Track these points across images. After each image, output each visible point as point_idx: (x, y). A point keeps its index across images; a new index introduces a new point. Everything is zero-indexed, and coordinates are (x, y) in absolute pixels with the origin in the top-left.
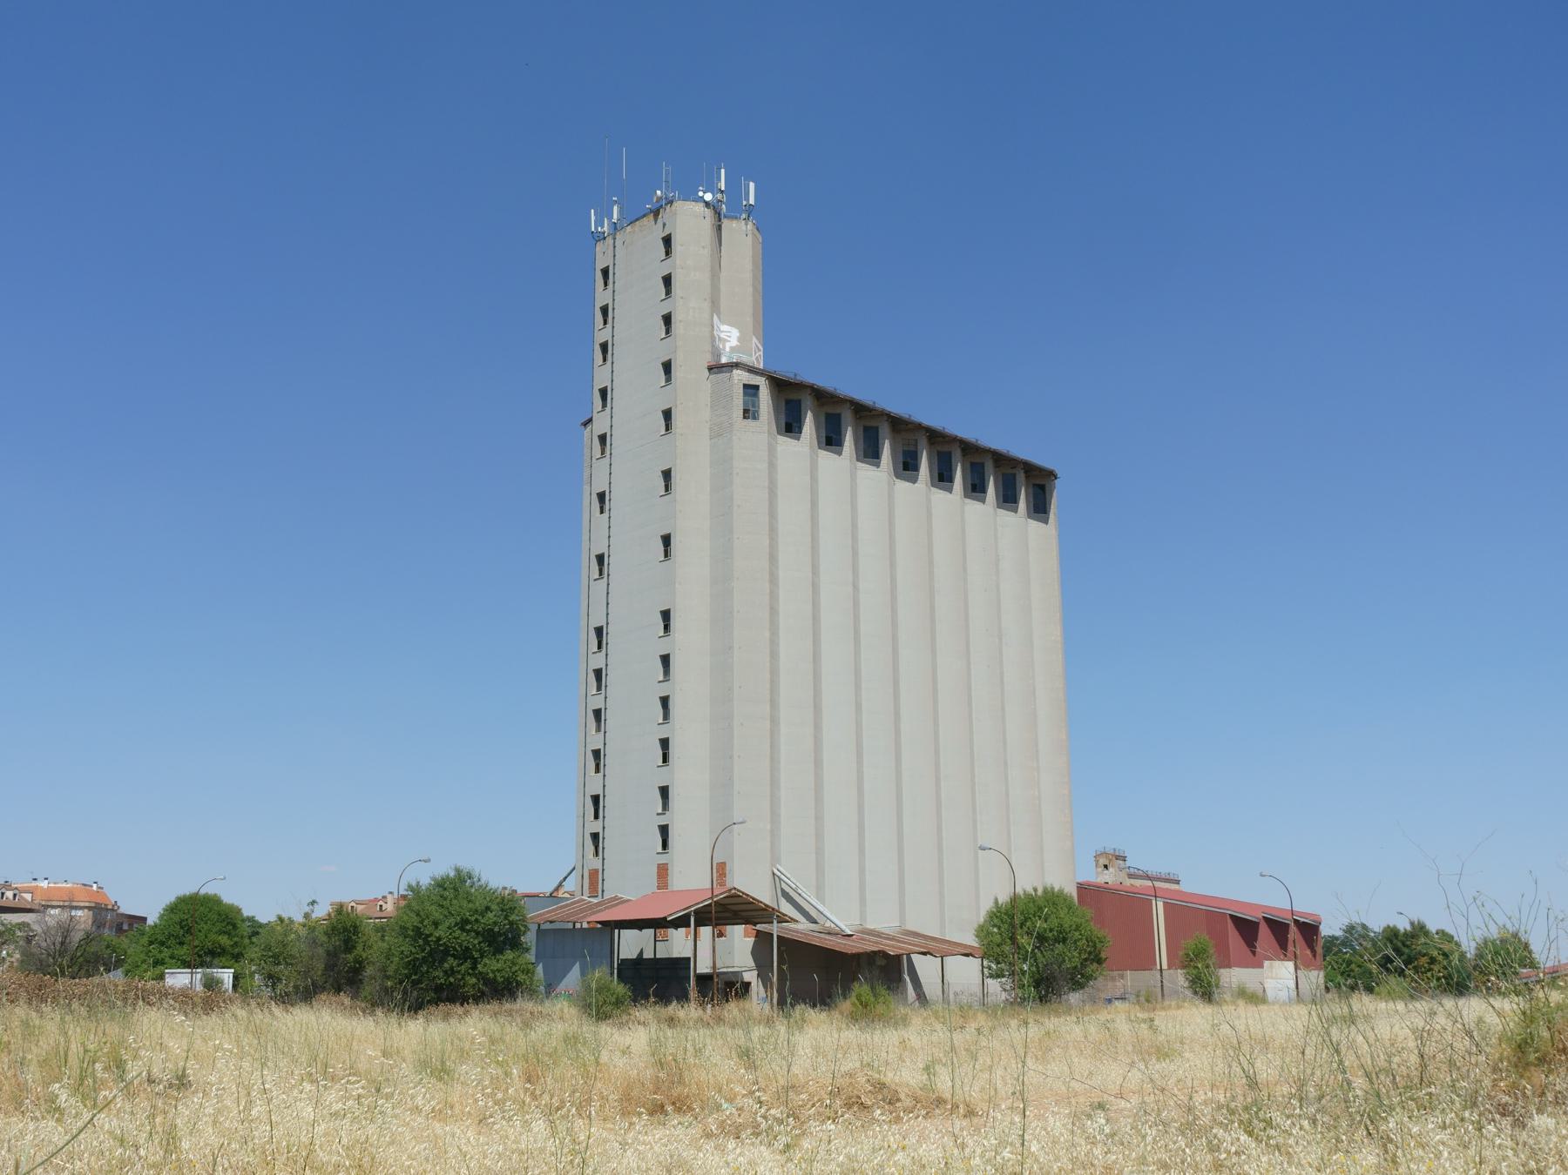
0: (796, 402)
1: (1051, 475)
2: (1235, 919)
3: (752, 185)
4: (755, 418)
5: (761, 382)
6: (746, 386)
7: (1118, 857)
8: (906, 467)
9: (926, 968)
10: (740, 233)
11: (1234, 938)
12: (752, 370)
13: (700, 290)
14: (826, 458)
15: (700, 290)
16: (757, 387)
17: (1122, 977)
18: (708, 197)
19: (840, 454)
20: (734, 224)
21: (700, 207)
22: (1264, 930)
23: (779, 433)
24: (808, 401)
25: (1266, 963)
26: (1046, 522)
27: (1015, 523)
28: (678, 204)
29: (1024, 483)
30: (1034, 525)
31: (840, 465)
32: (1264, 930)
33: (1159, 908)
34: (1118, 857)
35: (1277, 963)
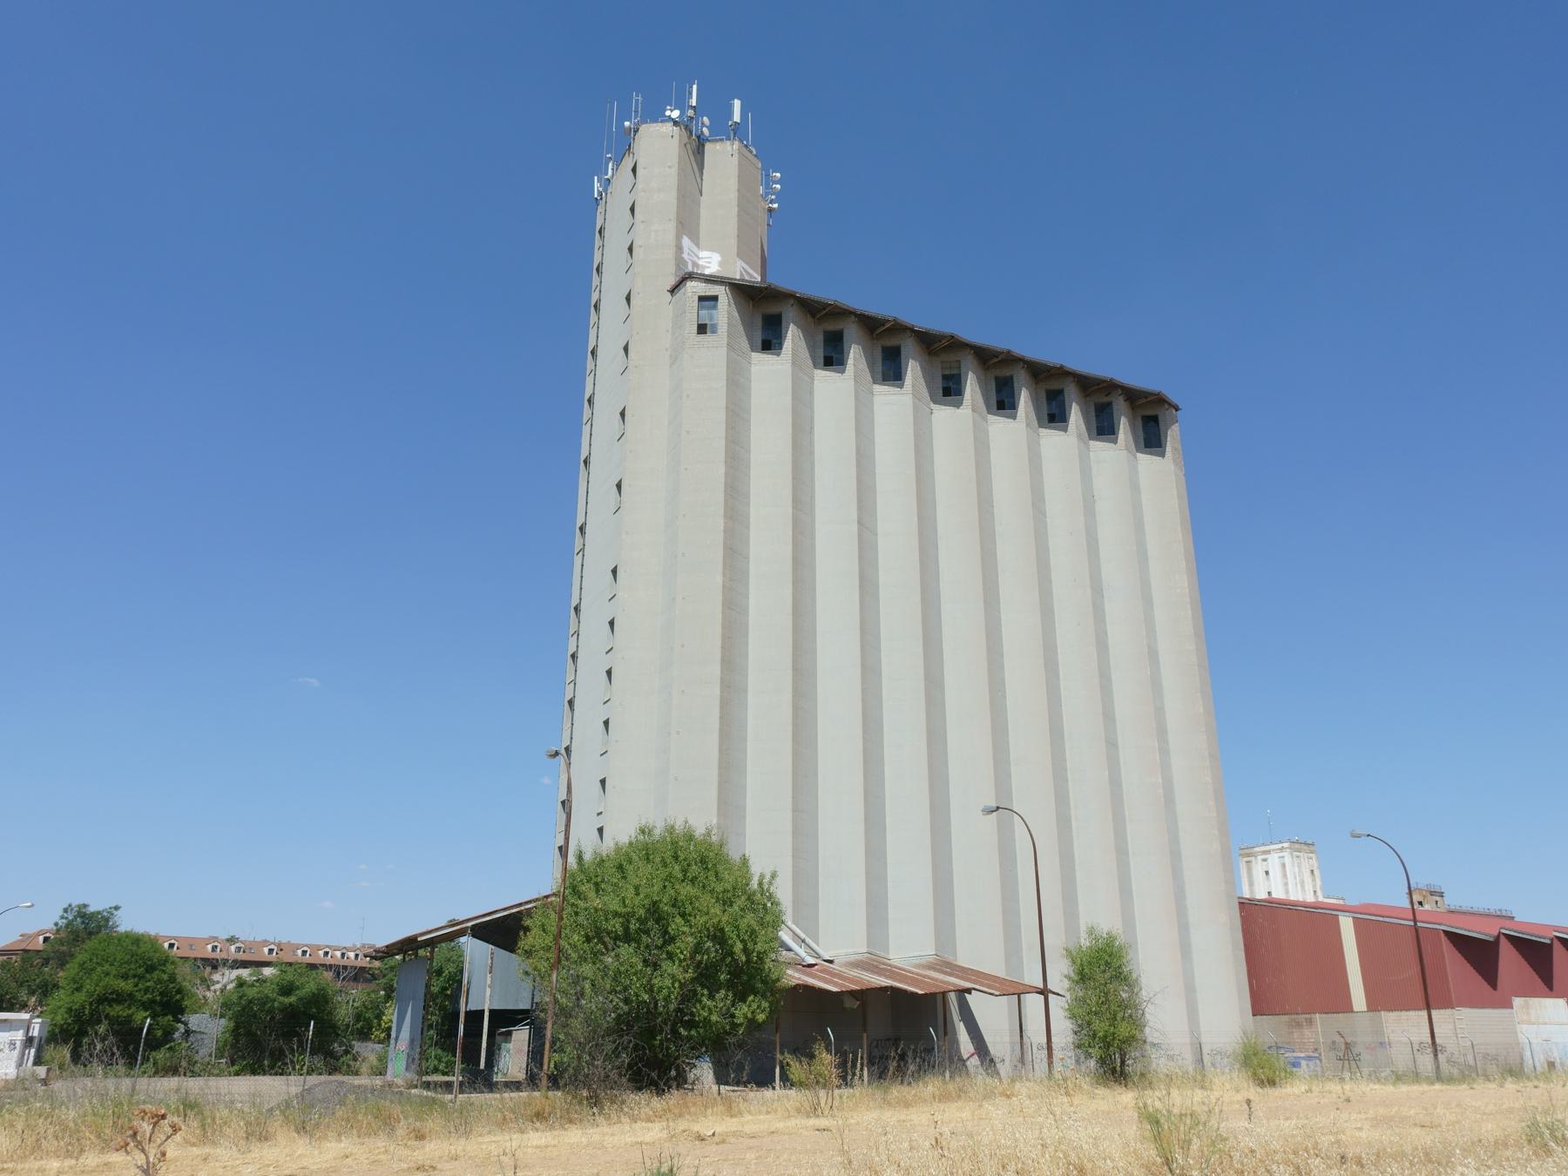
0: (765, 311)
1: (1160, 400)
2: (1454, 938)
3: (737, 103)
4: (714, 331)
5: (721, 291)
6: (701, 299)
7: (1432, 893)
8: (947, 392)
9: (990, 1012)
10: (724, 157)
11: (1455, 965)
12: (710, 280)
13: (678, 209)
14: (1100, 448)
15: (678, 209)
16: (715, 298)
17: (1310, 1022)
18: (675, 114)
19: (1014, 417)
20: (718, 146)
21: (669, 126)
22: (1507, 954)
23: (816, 366)
24: (851, 331)
25: (1518, 1002)
26: (1163, 455)
27: (1115, 457)
28: (643, 128)
29: (1150, 419)
30: (1146, 461)
31: (1012, 433)
32: (1507, 954)
33: (1347, 925)
34: (1432, 893)
35: (1535, 1002)
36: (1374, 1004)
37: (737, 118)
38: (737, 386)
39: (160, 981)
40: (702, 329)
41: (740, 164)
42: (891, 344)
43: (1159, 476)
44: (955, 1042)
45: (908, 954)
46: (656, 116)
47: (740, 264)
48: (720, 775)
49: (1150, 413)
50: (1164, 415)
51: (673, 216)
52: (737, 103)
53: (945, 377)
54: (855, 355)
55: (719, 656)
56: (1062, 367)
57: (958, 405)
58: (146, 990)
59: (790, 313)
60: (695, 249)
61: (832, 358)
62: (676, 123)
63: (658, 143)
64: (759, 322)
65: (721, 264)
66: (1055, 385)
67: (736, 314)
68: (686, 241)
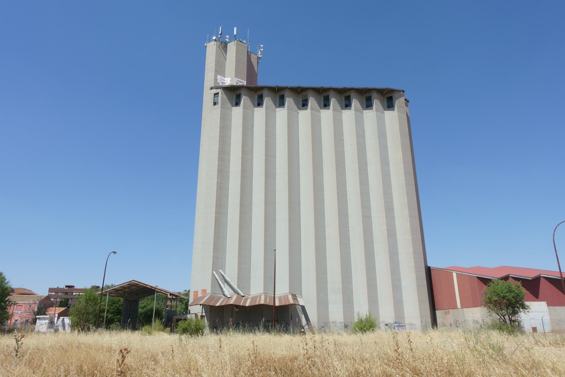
3: (235, 29)
16: (218, 93)
29: (389, 98)
36: (462, 307)
37: (235, 33)
38: (359, 123)
39: (116, 306)
40: (215, 104)
41: (237, 48)
42: (345, 97)
43: (393, 119)
44: (300, 321)
45: (282, 293)
46: (210, 41)
47: (236, 79)
48: (214, 241)
49: (390, 95)
50: (395, 95)
51: (214, 70)
52: (235, 29)
53: (303, 100)
54: (333, 102)
55: (215, 204)
56: (344, 88)
57: (306, 109)
58: (112, 309)
59: (374, 95)
60: (223, 78)
61: (326, 105)
62: (215, 40)
63: (212, 48)
64: (385, 100)
65: (231, 81)
66: (347, 94)
67: (225, 97)
68: (219, 77)
